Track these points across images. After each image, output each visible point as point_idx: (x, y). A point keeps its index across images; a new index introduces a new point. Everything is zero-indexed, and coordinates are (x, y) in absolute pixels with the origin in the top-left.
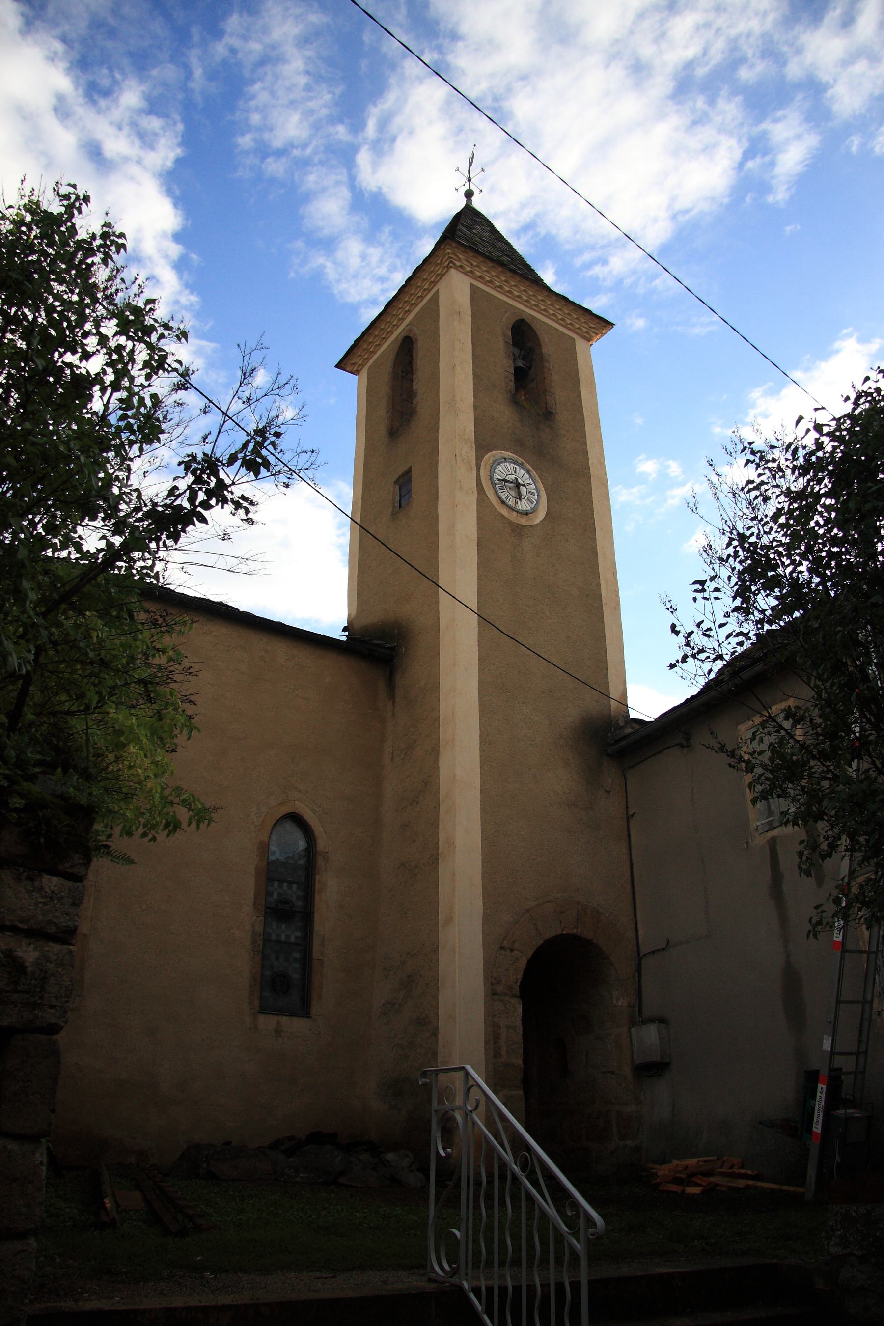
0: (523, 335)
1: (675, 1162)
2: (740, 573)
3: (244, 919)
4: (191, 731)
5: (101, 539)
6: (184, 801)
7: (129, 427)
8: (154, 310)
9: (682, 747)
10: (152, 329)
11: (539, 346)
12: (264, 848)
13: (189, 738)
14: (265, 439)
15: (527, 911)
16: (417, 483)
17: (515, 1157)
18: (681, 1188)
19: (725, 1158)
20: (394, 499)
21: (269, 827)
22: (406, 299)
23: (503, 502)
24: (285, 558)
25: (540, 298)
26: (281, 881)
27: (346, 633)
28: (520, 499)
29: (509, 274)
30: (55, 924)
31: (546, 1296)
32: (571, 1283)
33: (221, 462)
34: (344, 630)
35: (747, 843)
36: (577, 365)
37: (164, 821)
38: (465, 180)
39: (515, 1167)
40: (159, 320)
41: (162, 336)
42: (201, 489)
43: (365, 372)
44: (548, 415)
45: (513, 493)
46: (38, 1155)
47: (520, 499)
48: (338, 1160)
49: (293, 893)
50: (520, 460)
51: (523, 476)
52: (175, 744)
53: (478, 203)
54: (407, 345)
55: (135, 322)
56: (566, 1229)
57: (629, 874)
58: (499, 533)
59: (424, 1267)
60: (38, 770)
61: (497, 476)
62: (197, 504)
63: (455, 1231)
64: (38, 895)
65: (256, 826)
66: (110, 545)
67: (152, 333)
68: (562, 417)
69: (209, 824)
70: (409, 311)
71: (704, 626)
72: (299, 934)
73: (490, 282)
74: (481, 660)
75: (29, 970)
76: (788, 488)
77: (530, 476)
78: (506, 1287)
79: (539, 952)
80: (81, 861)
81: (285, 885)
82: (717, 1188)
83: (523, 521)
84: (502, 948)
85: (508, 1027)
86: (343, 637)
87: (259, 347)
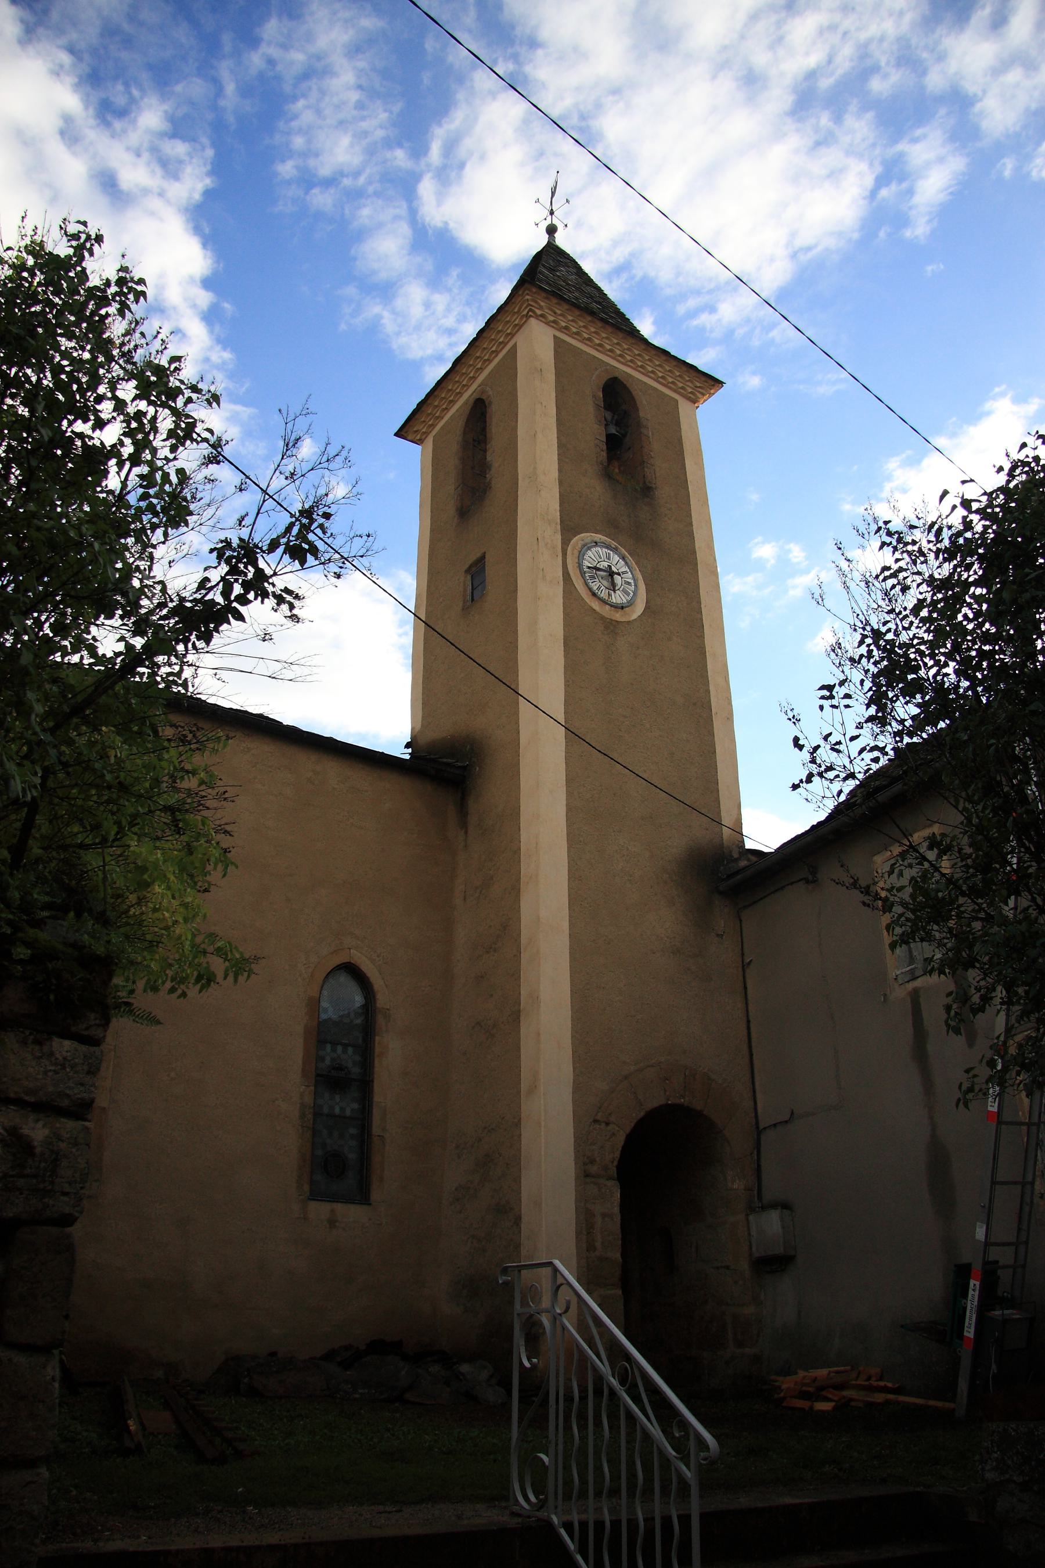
0: (616, 396)
1: (802, 1374)
2: (875, 676)
3: (291, 1088)
4: (226, 868)
6: (219, 949)
7: (151, 508)
9: (807, 881)
10: (178, 391)
12: (314, 1005)
13: (224, 876)
14: (312, 521)
15: (626, 1077)
20: (465, 591)
22: (478, 354)
23: (594, 594)
24: (337, 662)
25: (637, 352)
26: (334, 1044)
27: (410, 750)
28: (614, 591)
30: (68, 1096)
31: (650, 1532)
33: (261, 549)
34: (407, 746)
35: (885, 995)
37: (196, 973)
38: (547, 213)
39: (612, 1379)
41: (189, 401)
42: (236, 581)
43: (429, 441)
44: (647, 491)
45: (605, 583)
46: (49, 1369)
47: (614, 591)
48: (403, 1373)
49: (349, 1058)
50: (614, 544)
51: (617, 563)
53: (561, 240)
56: (674, 1453)
58: (589, 630)
60: (45, 914)
61: (586, 563)
62: (232, 598)
66: (130, 647)
67: (177, 396)
68: (664, 492)
69: (249, 976)
71: (833, 739)
72: (356, 1106)
73: (577, 333)
74: (569, 781)
75: (38, 1150)
76: (931, 576)
77: (626, 563)
78: (603, 1523)
79: (640, 1124)
80: (98, 1022)
81: (340, 1048)
82: (853, 1404)
83: (618, 616)
84: (596, 1121)
85: (604, 1215)
86: (405, 754)
87: (304, 412)
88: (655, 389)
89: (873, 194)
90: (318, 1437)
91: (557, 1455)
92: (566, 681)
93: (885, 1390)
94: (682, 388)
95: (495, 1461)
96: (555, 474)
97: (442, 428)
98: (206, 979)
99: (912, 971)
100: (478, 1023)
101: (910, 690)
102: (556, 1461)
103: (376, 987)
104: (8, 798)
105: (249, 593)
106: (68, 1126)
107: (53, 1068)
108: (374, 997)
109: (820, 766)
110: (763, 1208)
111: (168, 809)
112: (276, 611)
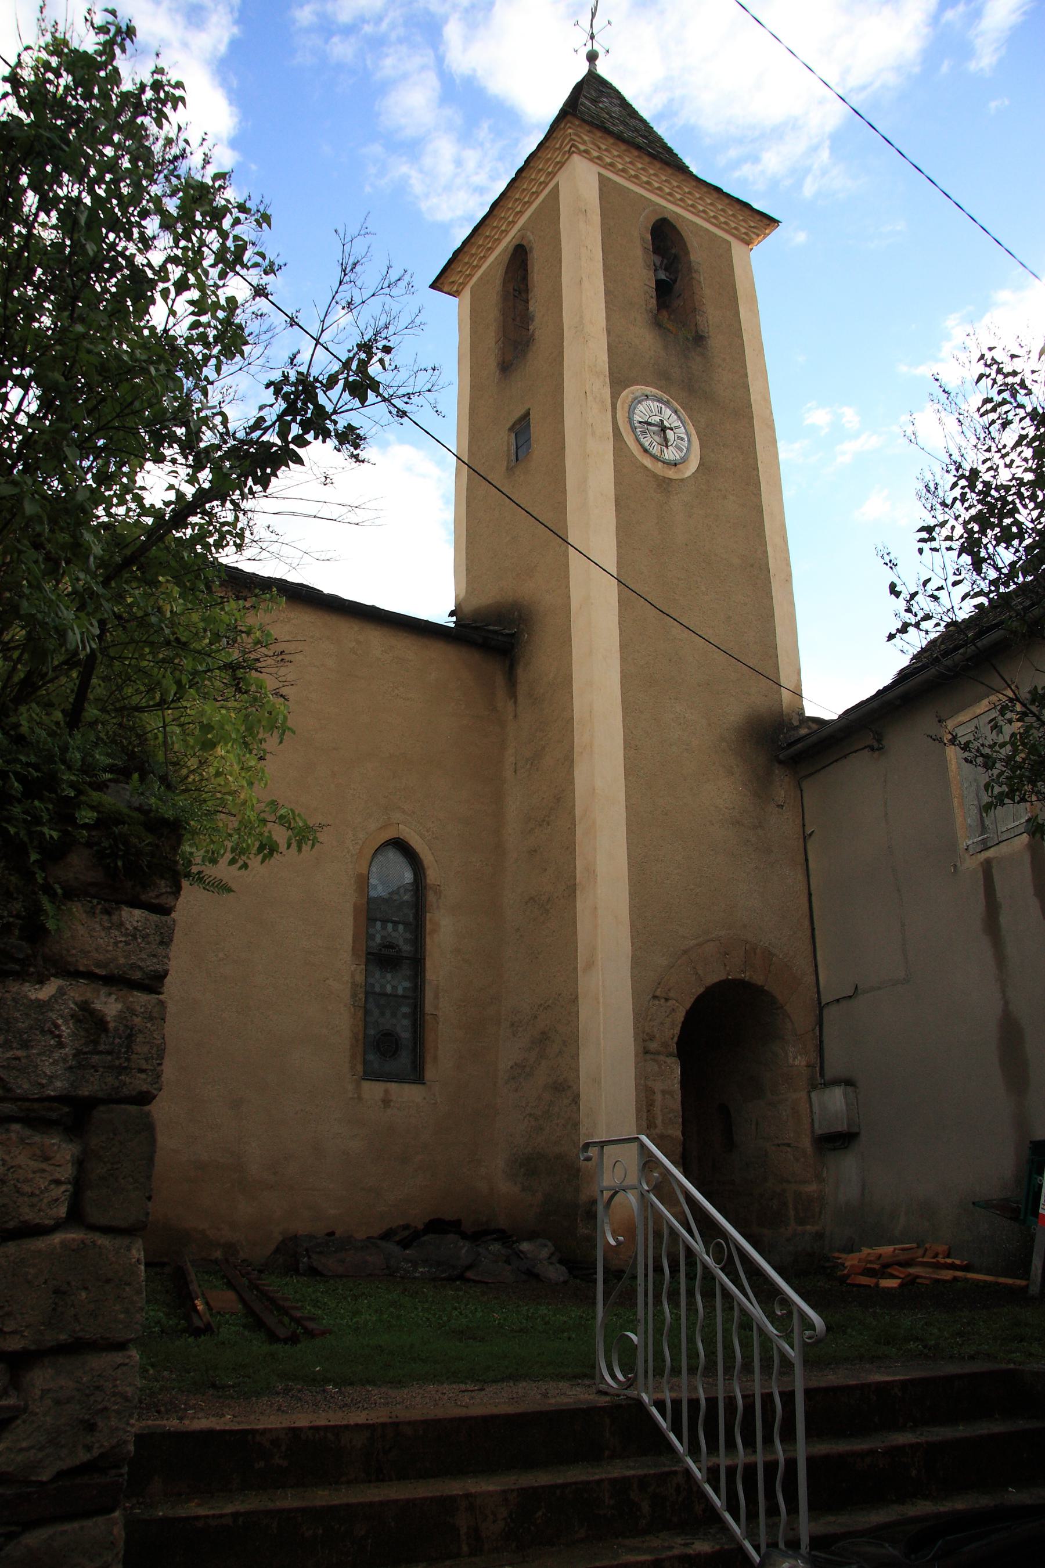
0: (665, 239)
1: (866, 1251)
2: (965, 523)
3: (343, 968)
4: (283, 733)
5: (167, 489)
6: (282, 817)
7: (203, 339)
8: (224, 188)
9: (872, 749)
10: (225, 211)
11: (687, 253)
12: (363, 882)
13: (281, 742)
14: (370, 356)
15: (685, 952)
16: (538, 429)
17: (706, 1244)
18: (874, 1280)
19: (927, 1245)
20: (509, 450)
21: (369, 857)
22: (517, 197)
23: (646, 451)
24: (372, 527)
25: (687, 190)
26: (384, 922)
27: (454, 619)
28: (667, 447)
29: (647, 159)
30: (140, 968)
31: (749, 1408)
32: (782, 1394)
33: (321, 382)
34: (452, 614)
35: (955, 866)
36: (734, 275)
37: (257, 844)
38: (587, 37)
39: (706, 1257)
40: (233, 201)
41: (237, 222)
42: (294, 420)
43: (467, 293)
44: (699, 339)
45: (657, 438)
46: (134, 1252)
47: (667, 447)
48: (464, 1251)
49: (400, 936)
50: (666, 397)
51: (669, 417)
52: (264, 750)
53: (603, 69)
54: (520, 256)
55: (200, 201)
56: (775, 1332)
57: (807, 905)
58: (642, 489)
59: (592, 1377)
60: (108, 776)
61: (637, 418)
62: (290, 439)
63: (629, 1334)
64: (117, 933)
65: (352, 856)
66: (180, 495)
67: (224, 216)
68: (716, 342)
69: (313, 845)
70: (521, 213)
71: (931, 587)
72: (407, 984)
73: (623, 170)
74: (623, 646)
75: (112, 1025)
76: (1035, 409)
77: (679, 417)
78: (698, 1401)
79: (699, 999)
80: (169, 890)
81: (390, 926)
82: (918, 1280)
83: (671, 473)
84: (655, 997)
85: (663, 1092)
86: (450, 622)
87: (363, 232)
88: (707, 230)
89: (935, 19)
90: (385, 1316)
91: (646, 1332)
92: (619, 543)
93: (952, 1267)
94: (736, 228)
95: (569, 1339)
96: (603, 323)
97: (481, 278)
98: (268, 849)
99: (984, 841)
100: (531, 898)
101: (1006, 538)
102: (646, 1338)
103: (426, 863)
104: (67, 650)
105: (308, 432)
106: (141, 999)
107: (123, 939)
108: (424, 874)
109: (916, 615)
110: (826, 1085)
111: (231, 667)
112: (339, 450)
